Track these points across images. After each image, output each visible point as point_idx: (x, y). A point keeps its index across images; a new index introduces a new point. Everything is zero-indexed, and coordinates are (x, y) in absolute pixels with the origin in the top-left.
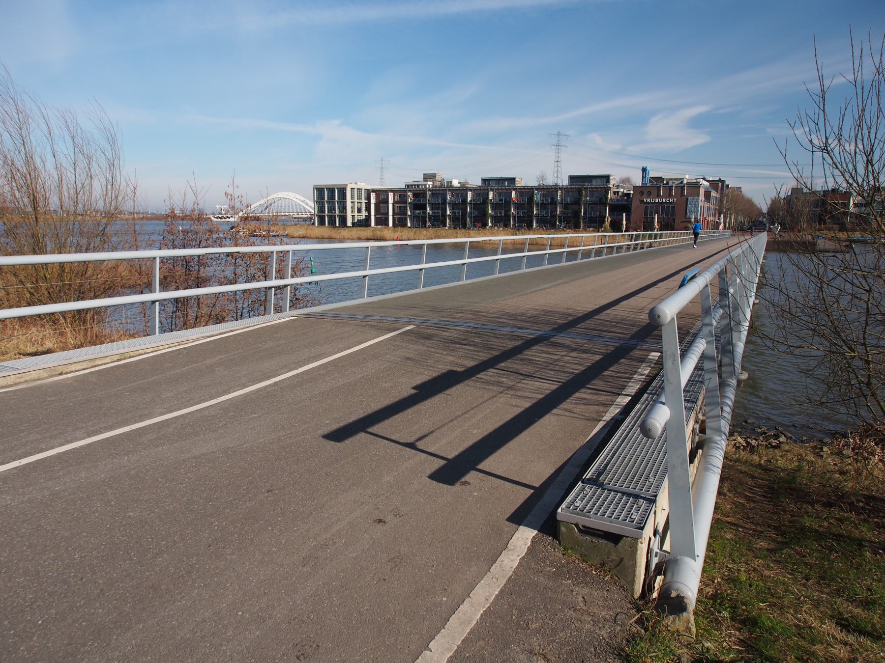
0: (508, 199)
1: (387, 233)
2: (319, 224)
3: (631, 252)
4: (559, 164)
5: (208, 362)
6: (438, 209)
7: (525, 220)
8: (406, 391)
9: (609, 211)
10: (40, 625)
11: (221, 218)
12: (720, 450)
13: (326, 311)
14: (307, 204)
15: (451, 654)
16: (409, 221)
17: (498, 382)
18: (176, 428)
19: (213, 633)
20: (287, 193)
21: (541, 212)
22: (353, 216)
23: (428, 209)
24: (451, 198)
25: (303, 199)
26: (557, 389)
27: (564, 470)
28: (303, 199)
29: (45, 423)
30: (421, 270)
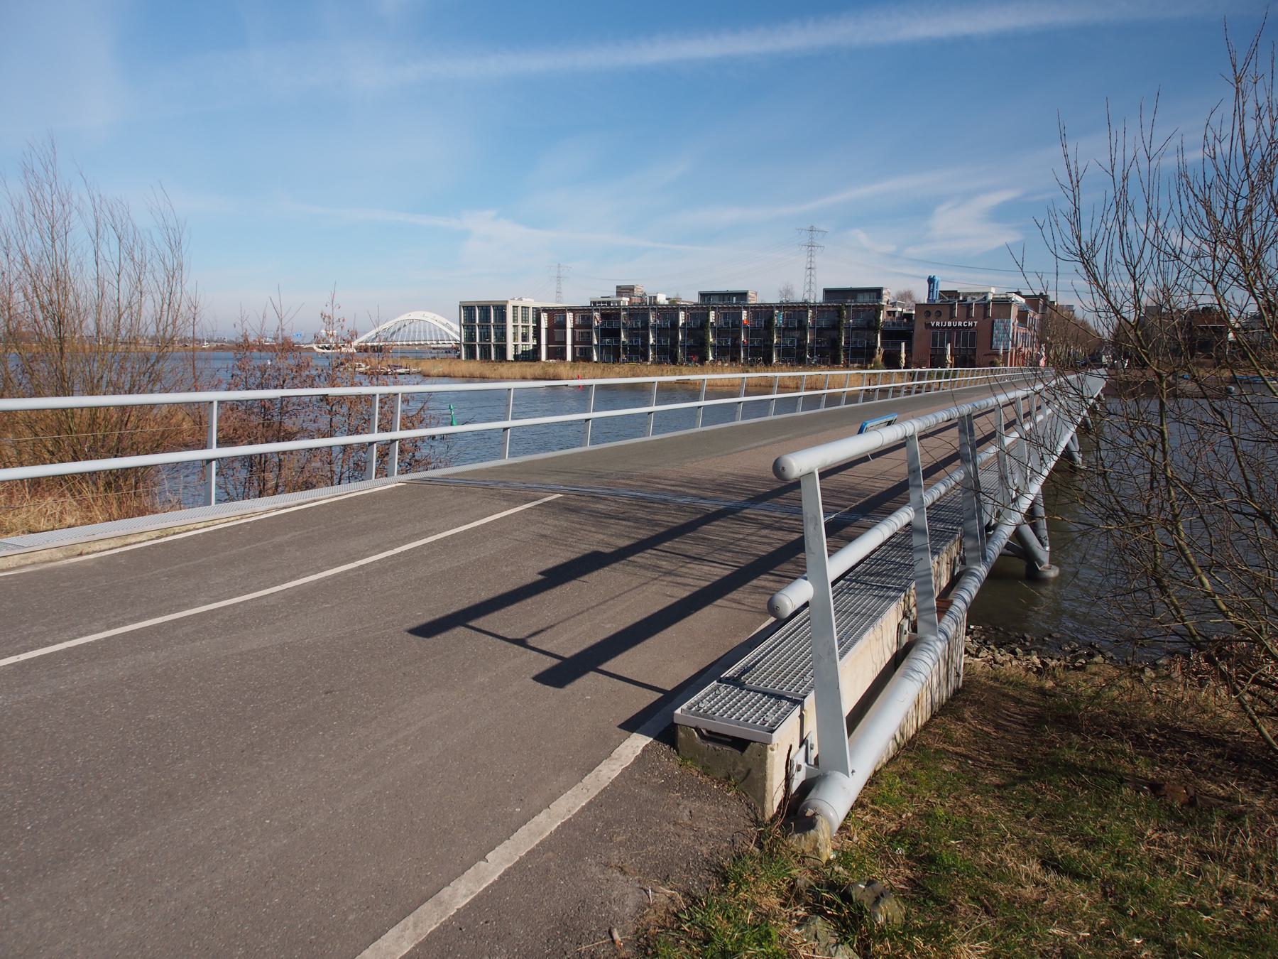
0: (737, 322)
1: (562, 369)
2: (466, 357)
3: (913, 395)
4: (813, 273)
5: (277, 540)
6: (637, 335)
7: (761, 352)
8: (530, 574)
9: (882, 339)
10: (29, 830)
11: (328, 349)
12: (931, 653)
13: (449, 475)
14: (451, 329)
15: (510, 865)
16: (595, 353)
17: (655, 566)
18: (222, 620)
19: (232, 841)
20: (423, 313)
21: (784, 340)
22: (515, 345)
23: (623, 336)
24: (655, 321)
25: (445, 321)
26: (730, 574)
27: (709, 672)
28: (445, 321)
29: (54, 613)
30: (587, 420)
